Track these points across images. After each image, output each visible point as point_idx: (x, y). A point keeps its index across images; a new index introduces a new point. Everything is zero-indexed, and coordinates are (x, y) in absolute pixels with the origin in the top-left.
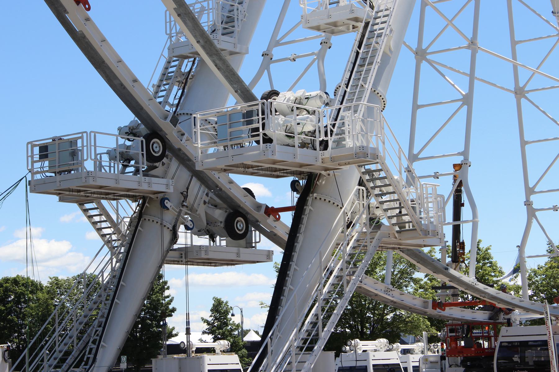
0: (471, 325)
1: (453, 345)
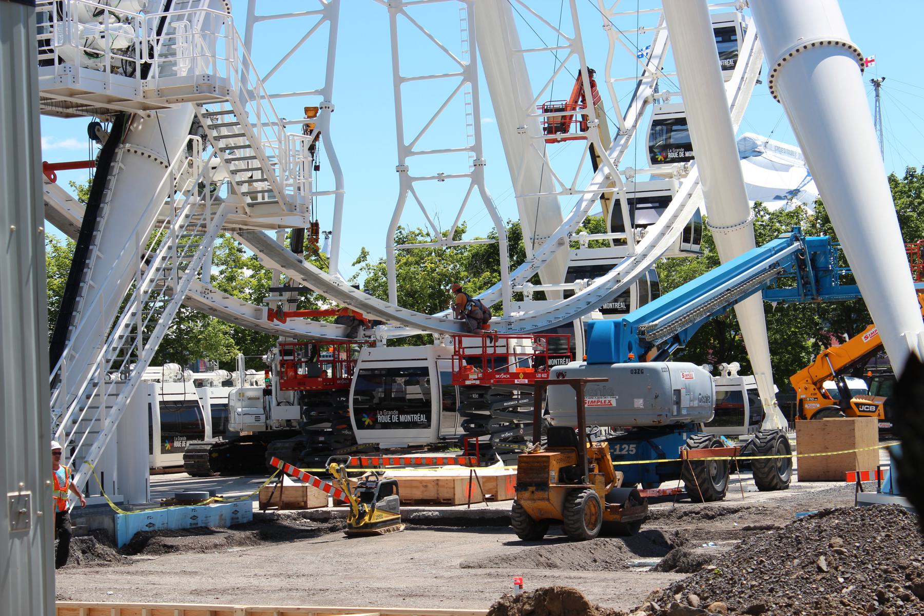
0: (318, 344)
1: (291, 373)
